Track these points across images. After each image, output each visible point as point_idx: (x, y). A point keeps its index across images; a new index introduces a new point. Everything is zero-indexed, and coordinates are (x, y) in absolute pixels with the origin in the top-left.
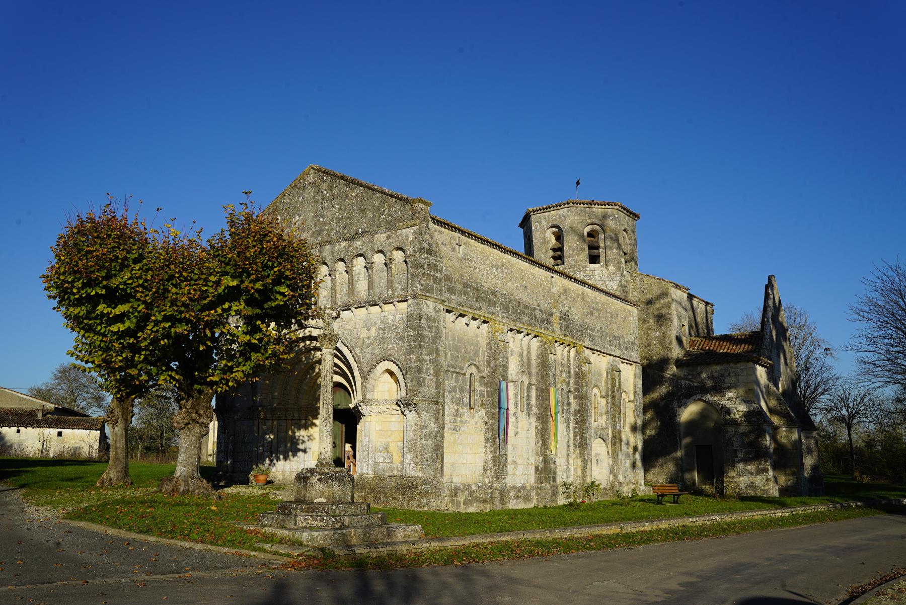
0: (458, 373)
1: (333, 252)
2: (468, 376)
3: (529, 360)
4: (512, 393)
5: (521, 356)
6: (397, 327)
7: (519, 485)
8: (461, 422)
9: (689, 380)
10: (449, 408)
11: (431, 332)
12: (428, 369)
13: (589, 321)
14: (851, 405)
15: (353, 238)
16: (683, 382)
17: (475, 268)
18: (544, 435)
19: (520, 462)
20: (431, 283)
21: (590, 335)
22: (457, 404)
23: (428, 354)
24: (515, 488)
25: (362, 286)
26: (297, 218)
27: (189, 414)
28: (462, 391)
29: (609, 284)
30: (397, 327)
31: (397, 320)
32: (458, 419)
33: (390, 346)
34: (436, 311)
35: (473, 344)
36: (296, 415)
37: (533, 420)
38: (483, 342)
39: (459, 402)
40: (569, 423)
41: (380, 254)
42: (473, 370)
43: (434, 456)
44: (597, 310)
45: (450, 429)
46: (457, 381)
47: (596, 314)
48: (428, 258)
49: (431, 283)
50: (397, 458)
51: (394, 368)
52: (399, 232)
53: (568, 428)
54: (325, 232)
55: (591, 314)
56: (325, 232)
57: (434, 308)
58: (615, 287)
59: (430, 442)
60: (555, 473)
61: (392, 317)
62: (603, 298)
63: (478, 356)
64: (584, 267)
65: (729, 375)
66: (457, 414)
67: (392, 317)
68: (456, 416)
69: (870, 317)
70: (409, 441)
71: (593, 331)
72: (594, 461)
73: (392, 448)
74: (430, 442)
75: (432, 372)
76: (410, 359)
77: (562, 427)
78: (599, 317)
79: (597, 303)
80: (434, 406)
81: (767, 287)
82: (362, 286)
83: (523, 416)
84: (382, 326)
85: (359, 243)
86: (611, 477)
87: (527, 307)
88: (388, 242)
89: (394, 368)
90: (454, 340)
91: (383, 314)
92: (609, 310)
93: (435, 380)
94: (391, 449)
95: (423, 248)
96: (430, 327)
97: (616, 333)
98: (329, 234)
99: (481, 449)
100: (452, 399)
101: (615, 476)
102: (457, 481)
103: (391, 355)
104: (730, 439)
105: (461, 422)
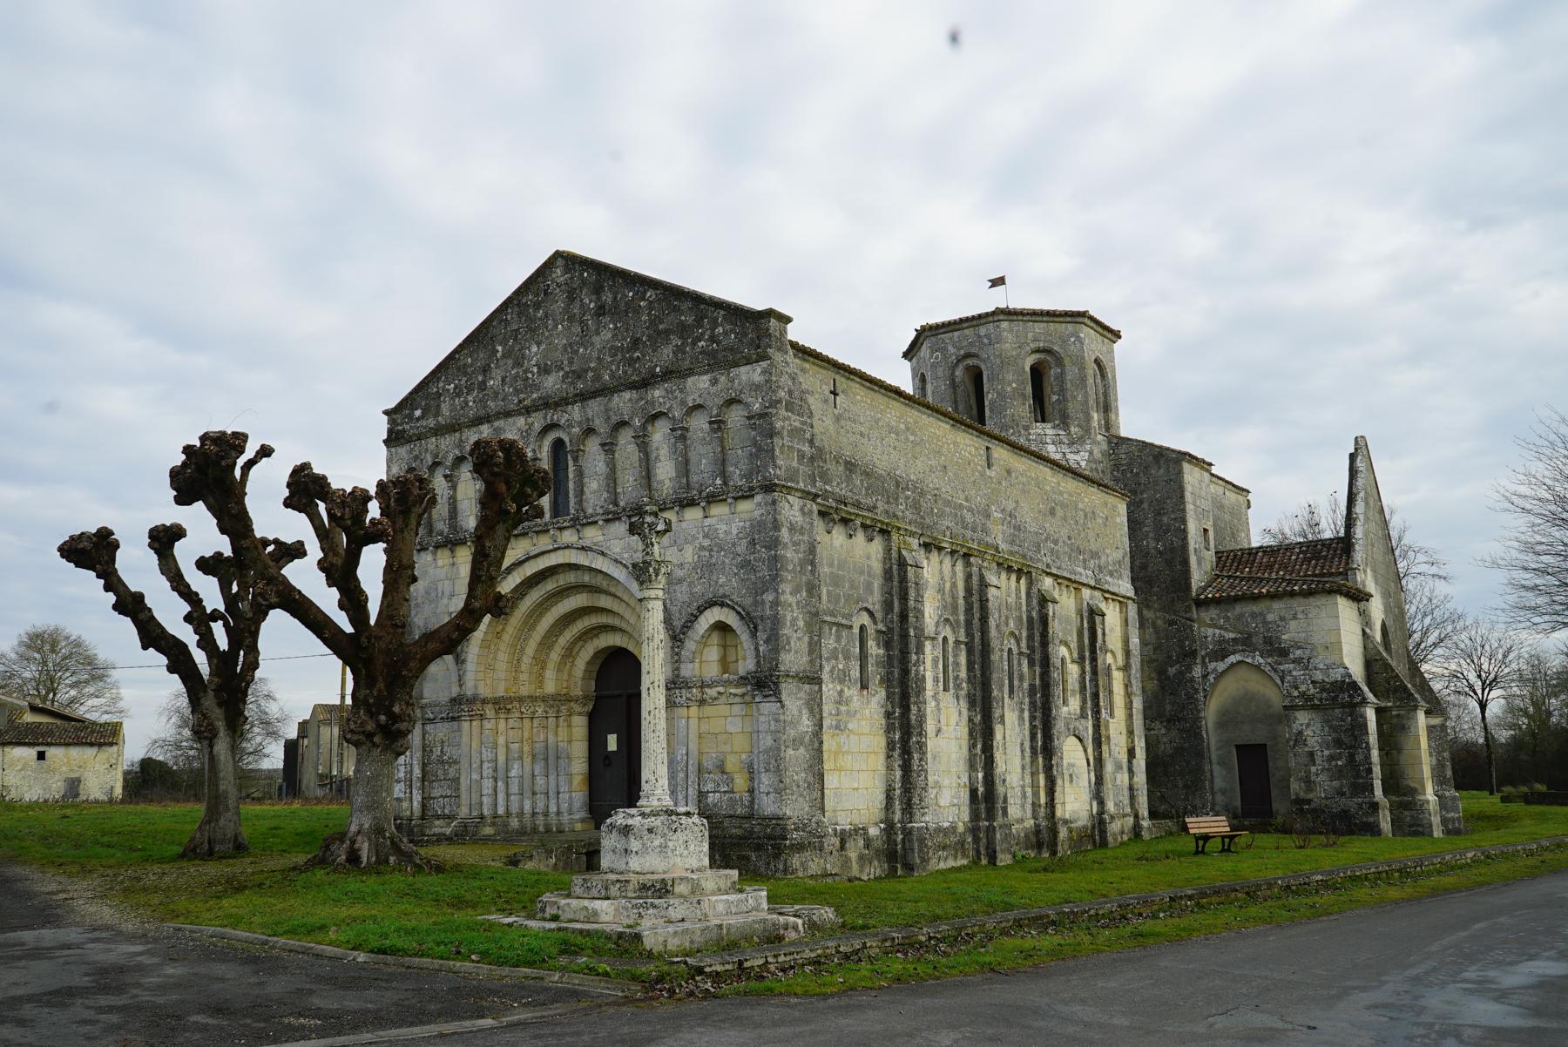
0: (838, 625)
1: (607, 410)
2: (856, 630)
3: (954, 598)
4: (929, 665)
5: (941, 590)
6: (734, 545)
7: (946, 825)
8: (848, 712)
9: (1221, 628)
10: (829, 689)
11: (796, 551)
12: (794, 620)
13: (1051, 526)
14: (1485, 667)
15: (645, 383)
16: (1210, 631)
17: (862, 435)
18: (983, 734)
19: (946, 782)
20: (795, 464)
21: (1052, 551)
22: (841, 682)
23: (795, 592)
24: (939, 830)
25: (665, 471)
26: (534, 349)
27: (372, 715)
28: (847, 657)
29: (1071, 457)
30: (734, 545)
31: (735, 532)
32: (843, 708)
33: (722, 580)
34: (804, 514)
35: (862, 573)
36: (540, 711)
37: (964, 704)
38: (877, 567)
39: (842, 678)
40: (1022, 711)
41: (734, 407)
42: (865, 619)
43: (810, 779)
44: (1063, 505)
45: (830, 727)
46: (838, 640)
47: (1060, 512)
48: (788, 418)
49: (795, 464)
50: (740, 782)
51: (731, 619)
52: (734, 371)
53: (1021, 718)
54: (590, 374)
55: (1052, 512)
56: (590, 374)
57: (802, 509)
58: (1083, 464)
59: (802, 750)
60: (1005, 800)
61: (724, 527)
62: (1070, 485)
63: (872, 593)
64: (1027, 428)
65: (1295, 618)
66: (841, 700)
67: (724, 527)
68: (839, 703)
69: (1528, 507)
70: (766, 751)
71: (1056, 542)
72: (1067, 777)
73: (732, 764)
74: (802, 750)
75: (801, 623)
76: (763, 602)
77: (1011, 717)
78: (1065, 519)
79: (1061, 493)
80: (807, 687)
81: (1353, 457)
82: (665, 471)
83: (948, 700)
84: (706, 543)
85: (657, 393)
86: (1095, 804)
87: (948, 503)
88: (713, 390)
89: (731, 619)
90: (831, 565)
91: (708, 522)
92: (1080, 506)
93: (806, 639)
94: (729, 767)
95: (779, 401)
96: (796, 544)
97: (1093, 548)
98: (597, 378)
99: (879, 762)
100: (832, 671)
101: (1101, 803)
102: (844, 823)
103: (725, 596)
104: (1300, 733)
105: (848, 712)
